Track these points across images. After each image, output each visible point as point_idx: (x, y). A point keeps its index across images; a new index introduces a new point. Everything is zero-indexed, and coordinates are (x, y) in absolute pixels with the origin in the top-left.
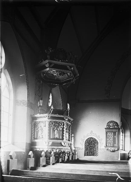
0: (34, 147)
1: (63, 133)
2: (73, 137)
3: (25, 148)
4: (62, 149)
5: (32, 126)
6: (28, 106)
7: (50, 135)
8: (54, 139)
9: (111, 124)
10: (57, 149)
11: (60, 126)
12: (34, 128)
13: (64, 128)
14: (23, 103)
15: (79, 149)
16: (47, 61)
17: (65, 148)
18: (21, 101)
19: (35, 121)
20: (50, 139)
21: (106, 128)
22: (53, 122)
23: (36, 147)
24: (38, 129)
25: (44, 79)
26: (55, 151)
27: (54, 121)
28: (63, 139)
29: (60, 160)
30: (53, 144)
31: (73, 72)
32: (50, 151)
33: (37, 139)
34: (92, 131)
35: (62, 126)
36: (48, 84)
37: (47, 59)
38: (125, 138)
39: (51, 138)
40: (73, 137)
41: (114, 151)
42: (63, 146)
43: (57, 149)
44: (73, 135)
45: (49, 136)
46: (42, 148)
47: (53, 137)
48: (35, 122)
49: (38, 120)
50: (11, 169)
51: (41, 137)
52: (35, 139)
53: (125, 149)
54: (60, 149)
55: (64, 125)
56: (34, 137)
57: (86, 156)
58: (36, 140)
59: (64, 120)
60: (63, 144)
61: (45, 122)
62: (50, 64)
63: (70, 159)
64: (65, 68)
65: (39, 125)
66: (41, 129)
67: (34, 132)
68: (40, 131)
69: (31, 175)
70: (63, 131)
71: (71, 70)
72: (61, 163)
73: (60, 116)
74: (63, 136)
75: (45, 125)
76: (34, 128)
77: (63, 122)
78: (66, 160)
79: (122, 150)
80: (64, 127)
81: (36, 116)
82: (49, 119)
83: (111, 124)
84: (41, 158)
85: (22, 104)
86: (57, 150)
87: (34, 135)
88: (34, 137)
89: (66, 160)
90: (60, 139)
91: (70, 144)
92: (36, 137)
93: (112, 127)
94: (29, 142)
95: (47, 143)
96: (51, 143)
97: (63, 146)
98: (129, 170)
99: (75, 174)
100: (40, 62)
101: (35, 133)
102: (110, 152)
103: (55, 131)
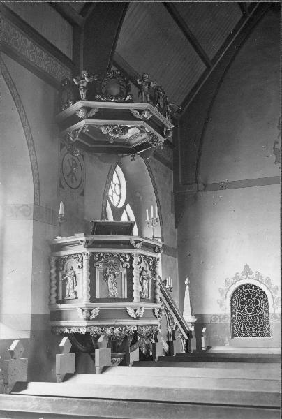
1: (130, 283)
2: (187, 288)
3: (28, 327)
4: (129, 325)
6: (36, 219)
11: (122, 263)
13: (132, 268)
15: (216, 319)
16: (79, 104)
17: (140, 322)
19: (57, 254)
22: (101, 255)
24: (64, 276)
25: (94, 138)
26: (109, 331)
27: (104, 253)
28: (130, 298)
29: (134, 356)
31: (153, 122)
32: (96, 334)
33: (63, 302)
34: (247, 267)
35: (128, 264)
36: (100, 154)
37: (78, 98)
40: (187, 288)
43: (116, 326)
44: (187, 281)
46: (75, 327)
47: (104, 296)
48: (59, 257)
51: (72, 296)
54: (125, 326)
55: (131, 261)
56: (57, 297)
57: (235, 338)
58: (62, 306)
59: (132, 247)
61: (80, 256)
62: (88, 109)
64: (127, 115)
66: (73, 274)
67: (57, 284)
68: (70, 279)
69: (98, 403)
70: (130, 276)
71: (145, 120)
72: (135, 364)
73: (114, 239)
74: (130, 290)
75: (80, 264)
77: (130, 254)
78: (159, 353)
80: (134, 266)
81: (60, 240)
82: (88, 247)
84: (58, 356)
86: (116, 331)
87: (57, 291)
88: (57, 297)
89: (159, 353)
91: (156, 312)
92: (60, 298)
96: (96, 311)
100: (66, 108)
101: (60, 283)
103: (107, 280)
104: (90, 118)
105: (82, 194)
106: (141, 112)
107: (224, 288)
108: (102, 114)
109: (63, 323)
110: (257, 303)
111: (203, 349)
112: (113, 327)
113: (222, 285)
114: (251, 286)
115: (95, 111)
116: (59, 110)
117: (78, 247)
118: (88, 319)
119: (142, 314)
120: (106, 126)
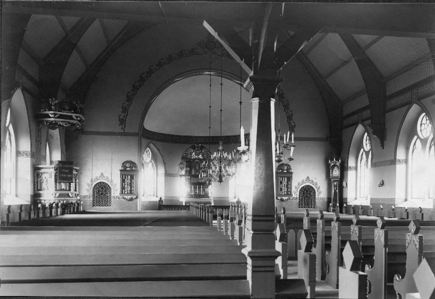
0: (38, 198)
5: (34, 177)
6: (31, 157)
7: (258, 231)
8: (61, 190)
9: (128, 165)
10: (64, 200)
12: (37, 178)
14: (26, 154)
18: (24, 152)
19: (38, 171)
20: (56, 190)
21: (121, 170)
23: (41, 198)
26: (62, 202)
30: (60, 196)
33: (41, 190)
38: (158, 177)
39: (58, 189)
41: (131, 200)
42: (70, 197)
45: (56, 187)
49: (42, 171)
50: (22, 219)
52: (38, 190)
53: (18, 193)
56: (37, 188)
58: (40, 192)
60: (70, 195)
62: (55, 114)
63: (76, 211)
65: (44, 176)
74: (70, 187)
76: (37, 178)
79: (154, 196)
83: (128, 165)
85: (25, 155)
86: (65, 202)
87: (37, 186)
88: (37, 188)
90: (66, 190)
92: (39, 188)
93: (129, 169)
94: (32, 194)
95: (54, 195)
96: (57, 195)
97: (70, 197)
98: (41, 165)
99: (220, 43)
102: (127, 201)
104: (56, 118)
105: (41, 143)
106: (76, 117)
107: (295, 191)
108: (61, 117)
109: (41, 198)
110: (106, 191)
111: (274, 100)
112: (63, 200)
113: (89, 181)
114: (104, 183)
115: (58, 115)
116: (38, 110)
117: (50, 169)
118: (55, 197)
119: (285, 160)
120: (62, 122)
